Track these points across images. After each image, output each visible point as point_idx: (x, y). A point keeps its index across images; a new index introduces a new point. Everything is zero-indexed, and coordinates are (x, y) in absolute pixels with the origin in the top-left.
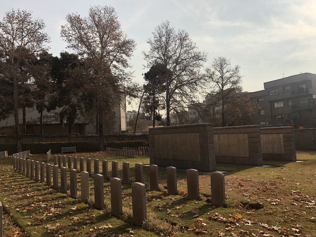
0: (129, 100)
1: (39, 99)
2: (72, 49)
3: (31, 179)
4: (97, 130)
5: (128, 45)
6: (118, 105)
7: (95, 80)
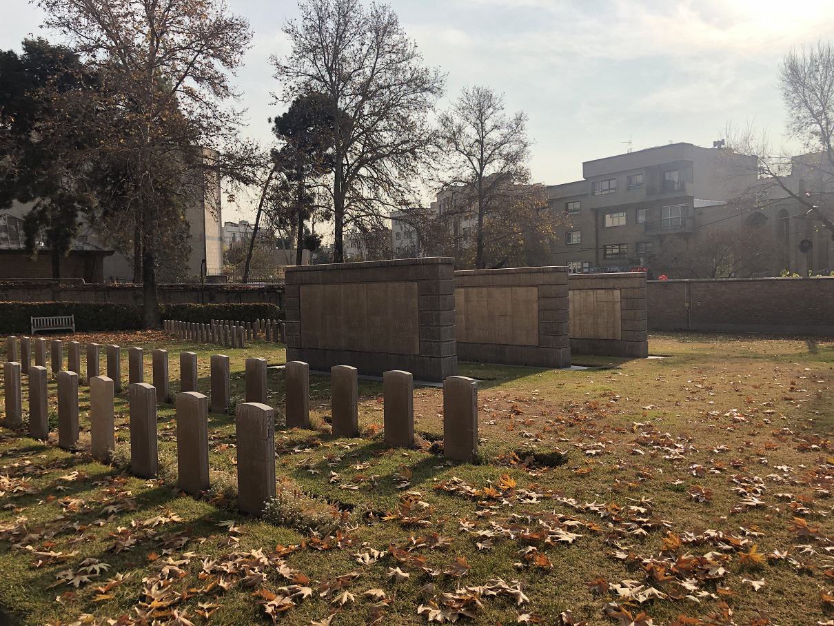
4: (137, 269)
6: (198, 203)
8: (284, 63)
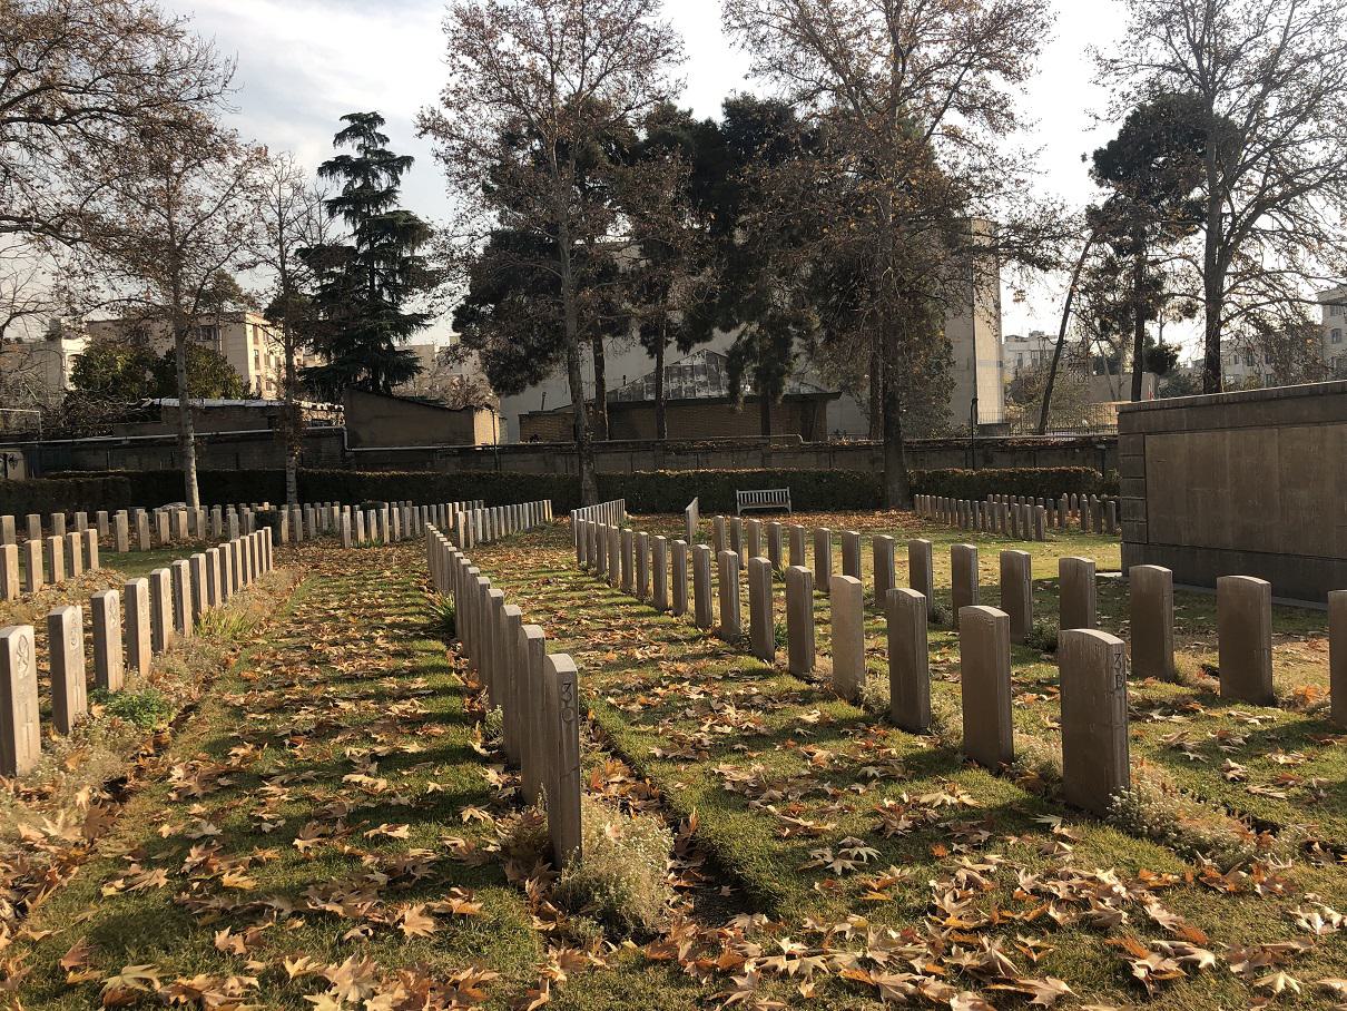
0: (1016, 284)
1: (649, 301)
2: (768, 77)
3: (641, 602)
4: (874, 419)
5: (1017, 25)
6: (967, 309)
7: (865, 204)
8: (1108, 56)
